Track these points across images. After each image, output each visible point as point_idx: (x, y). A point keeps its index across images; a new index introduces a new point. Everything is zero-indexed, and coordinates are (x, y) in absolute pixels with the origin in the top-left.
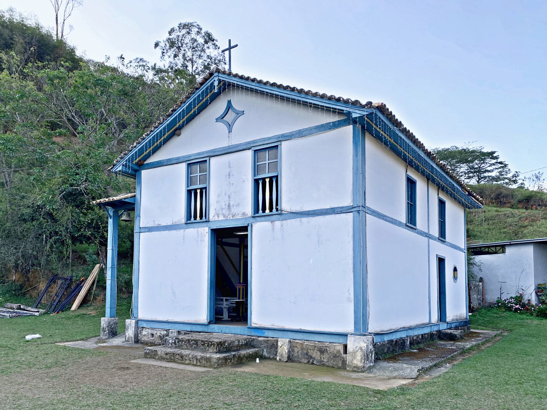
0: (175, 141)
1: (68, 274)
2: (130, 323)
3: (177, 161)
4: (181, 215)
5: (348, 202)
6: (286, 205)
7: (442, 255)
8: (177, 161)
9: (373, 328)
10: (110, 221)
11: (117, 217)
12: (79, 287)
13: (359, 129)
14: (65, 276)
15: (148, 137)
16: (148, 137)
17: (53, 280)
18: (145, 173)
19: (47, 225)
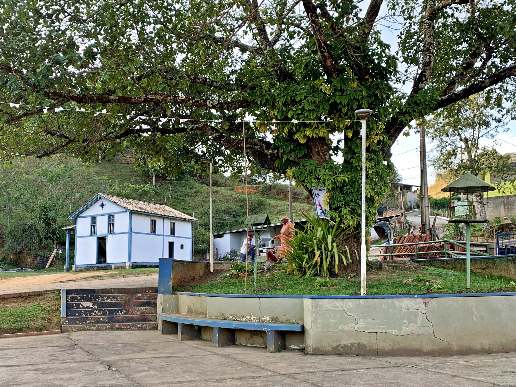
0: (88, 210)
1: (42, 254)
2: (74, 266)
3: (88, 217)
4: (89, 233)
5: (128, 231)
6: (115, 231)
7: (171, 241)
8: (88, 217)
9: (133, 260)
10: (67, 234)
11: (70, 233)
12: (48, 259)
13: (30, 340)
14: (41, 254)
15: (80, 210)
16: (80, 210)
17: (36, 256)
18: (79, 220)
19: (35, 233)
